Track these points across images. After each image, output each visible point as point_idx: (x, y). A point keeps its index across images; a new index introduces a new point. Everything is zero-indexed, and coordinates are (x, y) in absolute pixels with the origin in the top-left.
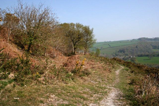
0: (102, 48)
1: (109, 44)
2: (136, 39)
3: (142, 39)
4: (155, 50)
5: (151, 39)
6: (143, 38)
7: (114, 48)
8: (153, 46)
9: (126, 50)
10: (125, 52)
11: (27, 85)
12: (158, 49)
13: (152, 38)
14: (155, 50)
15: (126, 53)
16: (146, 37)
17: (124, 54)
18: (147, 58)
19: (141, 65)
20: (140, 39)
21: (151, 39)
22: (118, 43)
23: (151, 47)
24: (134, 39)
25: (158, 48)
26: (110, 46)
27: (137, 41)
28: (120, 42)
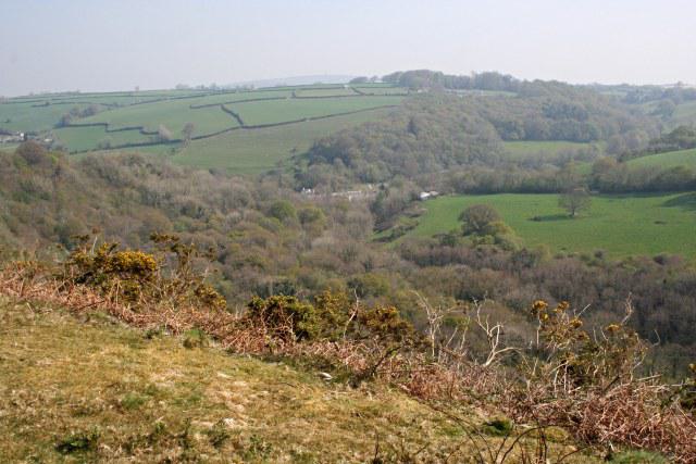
0: (188, 129)
1: (226, 106)
2: (375, 78)
3: (418, 78)
4: (519, 149)
5: (461, 78)
6: (418, 73)
7: (267, 131)
8: (496, 124)
9: (354, 150)
10: (353, 161)
11: (552, 410)
12: (520, 139)
13: (467, 73)
14: (519, 149)
15: (362, 165)
16: (434, 68)
17: (349, 172)
18: (548, 204)
19: (319, 283)
20: (486, 81)
21: (463, 83)
22: (284, 98)
23: (490, 131)
24: (362, 75)
25: (523, 135)
26: (236, 116)
27: (384, 91)
28: (295, 92)
